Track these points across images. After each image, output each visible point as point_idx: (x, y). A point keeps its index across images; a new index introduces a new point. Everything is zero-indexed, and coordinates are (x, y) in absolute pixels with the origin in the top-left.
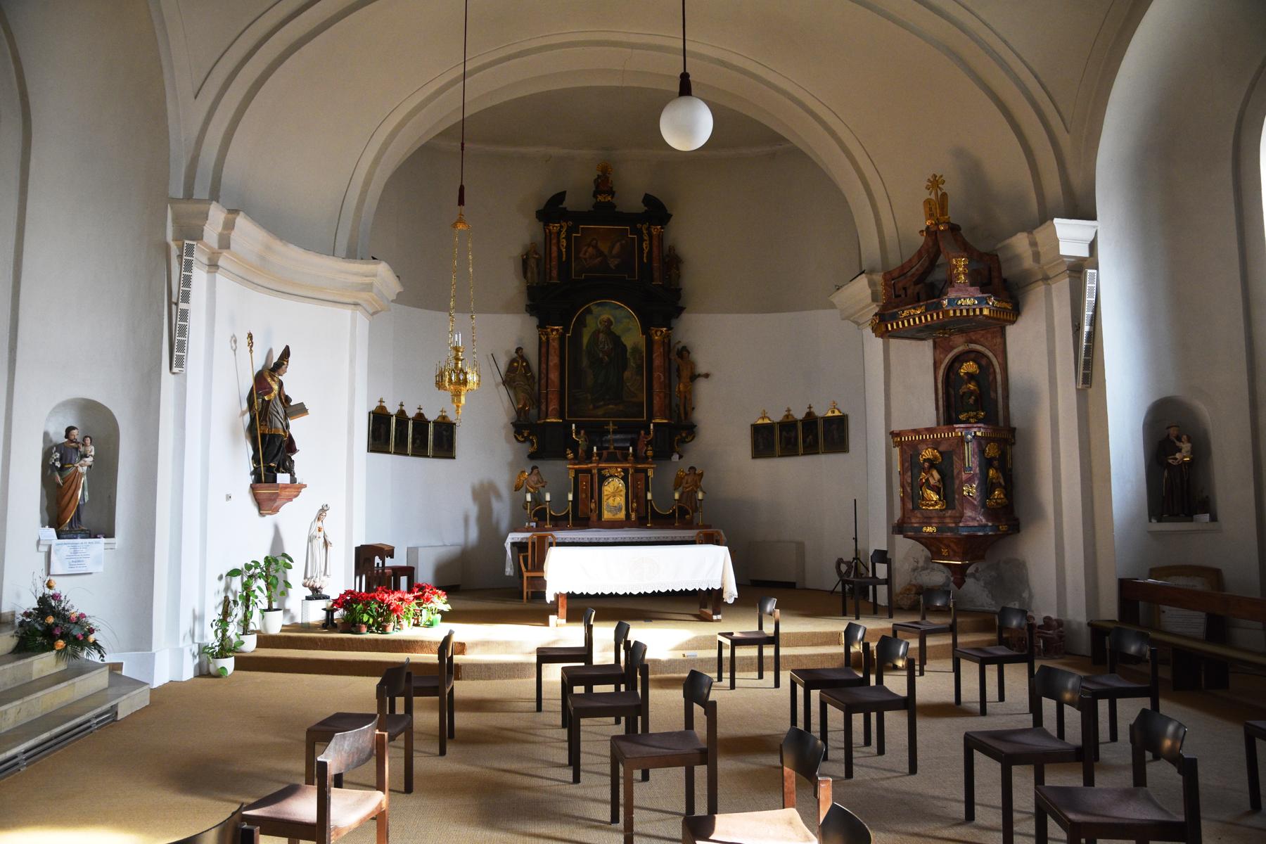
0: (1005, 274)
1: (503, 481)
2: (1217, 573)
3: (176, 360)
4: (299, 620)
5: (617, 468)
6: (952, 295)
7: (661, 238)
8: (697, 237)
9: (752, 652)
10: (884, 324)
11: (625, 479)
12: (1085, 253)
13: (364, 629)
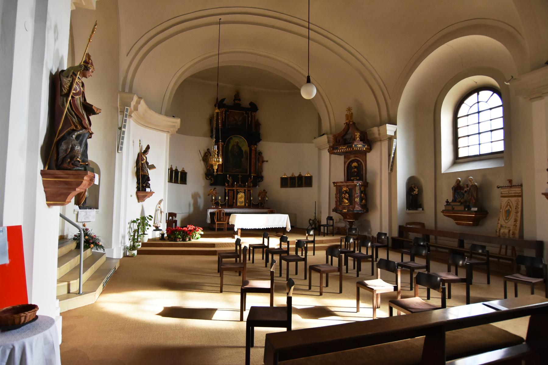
0: (368, 138)
1: (201, 192)
5: (242, 189)
6: (356, 143)
7: (255, 116)
8: (266, 117)
9: (312, 245)
11: (245, 193)
12: (393, 134)
13: (178, 240)
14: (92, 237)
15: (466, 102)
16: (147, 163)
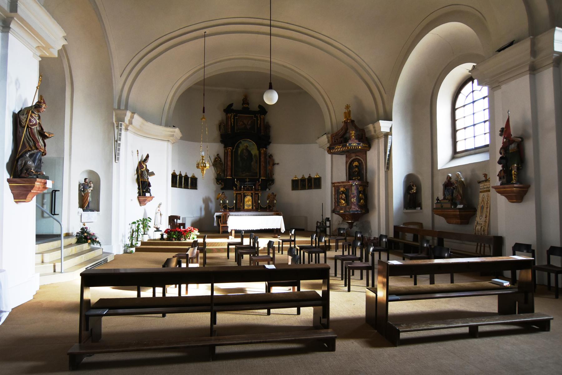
1: (212, 197)
2: (421, 224)
3: (117, 158)
4: (152, 238)
5: (249, 193)
7: (264, 119)
10: (330, 150)
11: (252, 196)
12: (389, 131)
14: (90, 234)
15: (462, 91)
16: (148, 171)
